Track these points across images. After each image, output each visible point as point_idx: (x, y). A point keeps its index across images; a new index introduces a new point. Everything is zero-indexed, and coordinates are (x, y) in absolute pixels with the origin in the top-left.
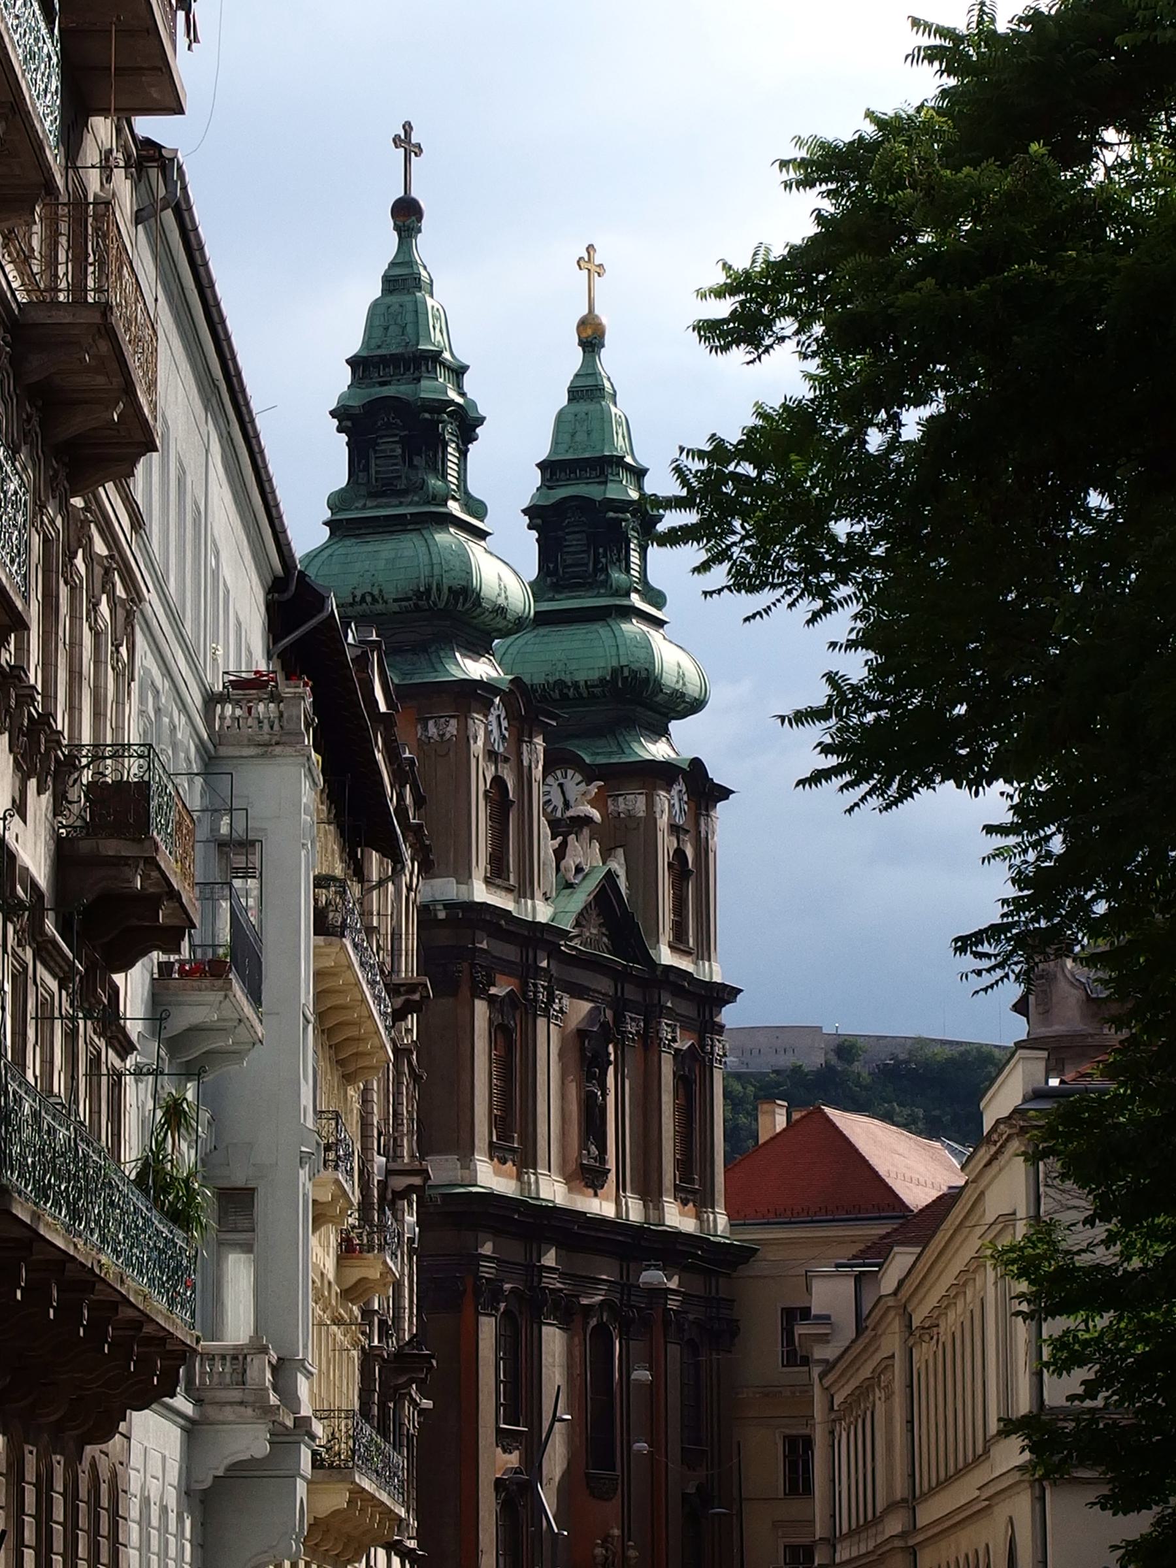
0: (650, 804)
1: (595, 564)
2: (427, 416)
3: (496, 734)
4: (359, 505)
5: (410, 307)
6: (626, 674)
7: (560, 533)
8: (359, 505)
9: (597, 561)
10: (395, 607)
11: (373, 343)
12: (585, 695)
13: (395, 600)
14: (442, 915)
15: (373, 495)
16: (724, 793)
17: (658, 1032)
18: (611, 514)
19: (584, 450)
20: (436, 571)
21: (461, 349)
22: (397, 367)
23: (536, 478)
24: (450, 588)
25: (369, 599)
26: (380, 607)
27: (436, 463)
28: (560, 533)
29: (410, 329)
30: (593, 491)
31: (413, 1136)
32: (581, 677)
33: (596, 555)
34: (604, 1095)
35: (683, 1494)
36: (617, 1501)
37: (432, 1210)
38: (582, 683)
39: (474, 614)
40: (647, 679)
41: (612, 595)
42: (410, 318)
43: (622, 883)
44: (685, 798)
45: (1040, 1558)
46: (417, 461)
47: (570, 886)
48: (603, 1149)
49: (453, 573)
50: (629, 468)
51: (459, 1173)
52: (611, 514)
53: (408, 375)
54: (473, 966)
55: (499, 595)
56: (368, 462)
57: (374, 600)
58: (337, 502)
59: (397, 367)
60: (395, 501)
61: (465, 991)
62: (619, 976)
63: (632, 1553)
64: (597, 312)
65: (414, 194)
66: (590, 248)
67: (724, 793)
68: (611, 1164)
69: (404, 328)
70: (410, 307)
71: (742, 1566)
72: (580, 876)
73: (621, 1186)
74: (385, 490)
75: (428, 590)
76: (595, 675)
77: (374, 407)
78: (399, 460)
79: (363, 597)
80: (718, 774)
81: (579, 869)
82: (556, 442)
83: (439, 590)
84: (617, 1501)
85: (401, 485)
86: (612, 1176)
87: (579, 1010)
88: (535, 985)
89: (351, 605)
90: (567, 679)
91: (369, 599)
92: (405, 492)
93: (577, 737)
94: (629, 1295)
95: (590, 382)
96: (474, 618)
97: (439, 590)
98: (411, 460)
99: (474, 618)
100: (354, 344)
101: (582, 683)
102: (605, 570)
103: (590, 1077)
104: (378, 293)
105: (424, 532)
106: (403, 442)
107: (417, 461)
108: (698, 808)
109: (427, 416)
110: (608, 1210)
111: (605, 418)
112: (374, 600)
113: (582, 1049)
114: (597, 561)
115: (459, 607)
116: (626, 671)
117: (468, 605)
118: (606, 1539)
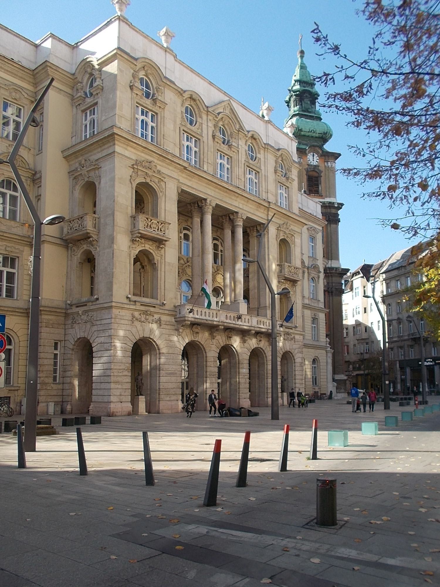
13: (319, 133)
25: (313, 131)
57: (314, 132)
89: (308, 132)
91: (313, 131)
112: (314, 132)
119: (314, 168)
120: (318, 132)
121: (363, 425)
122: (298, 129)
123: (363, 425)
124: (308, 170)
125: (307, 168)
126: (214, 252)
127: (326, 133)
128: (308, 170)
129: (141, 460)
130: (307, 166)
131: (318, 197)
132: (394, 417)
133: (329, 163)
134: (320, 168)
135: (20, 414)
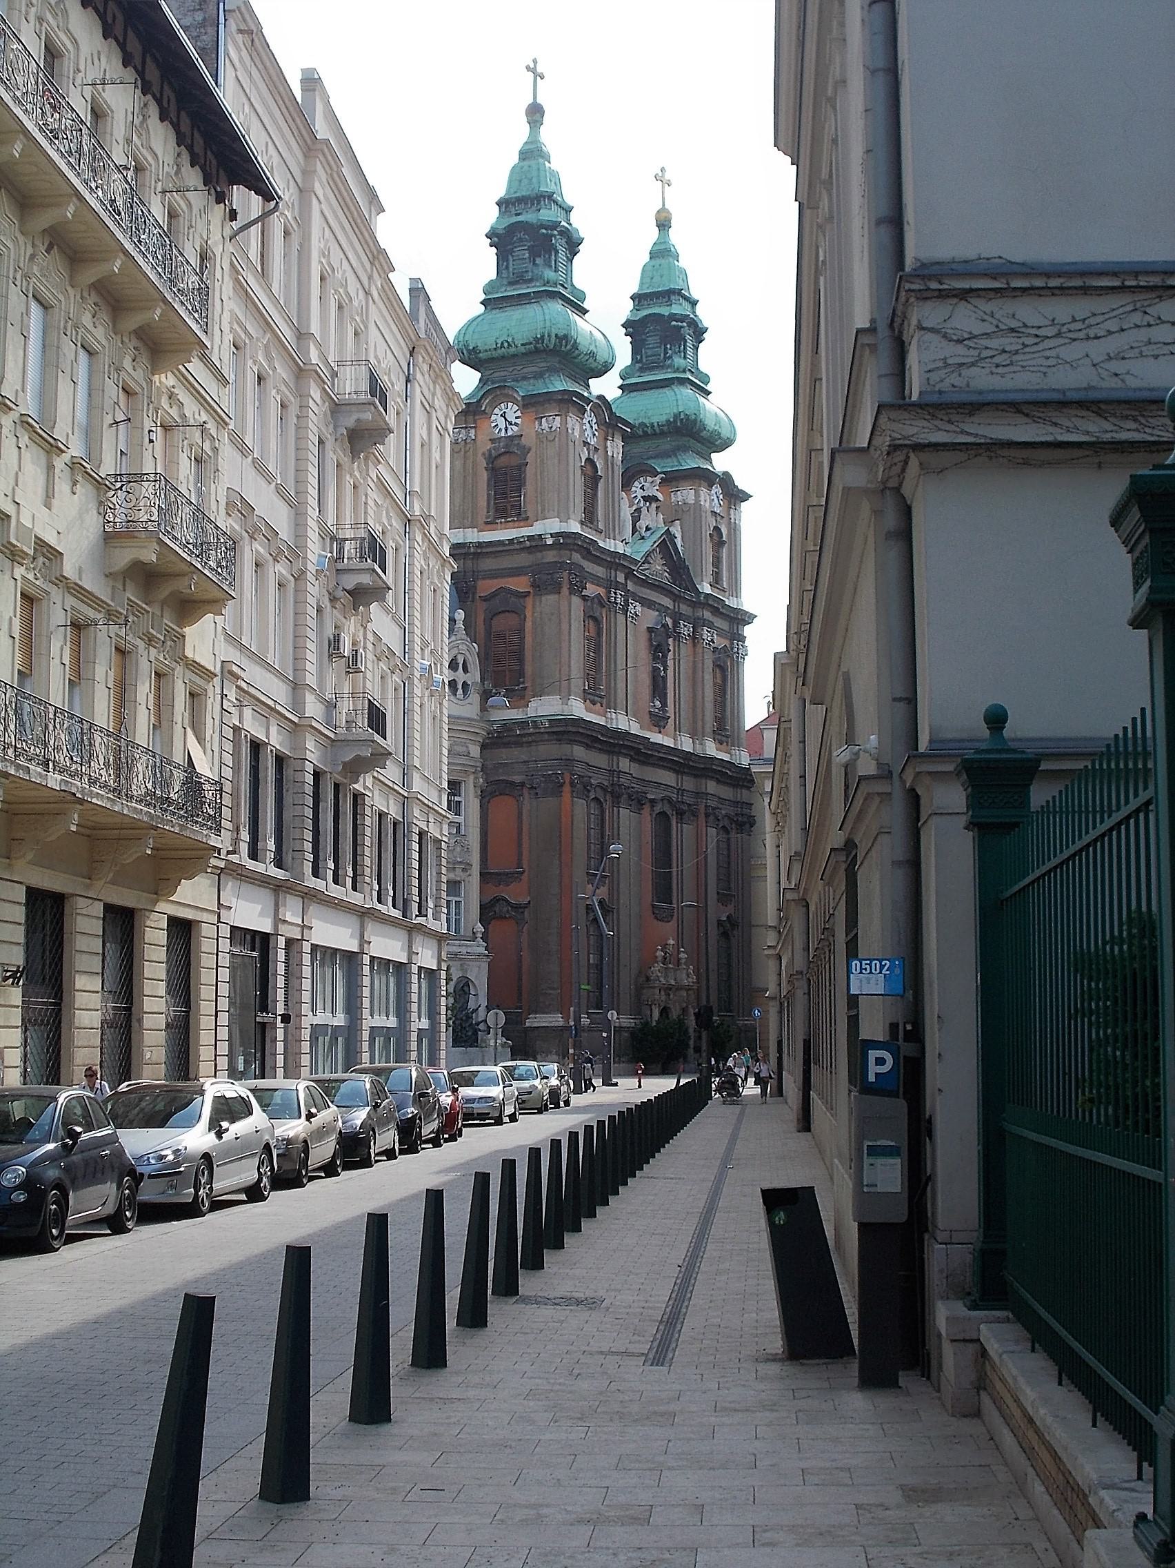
0: (697, 495)
1: (665, 354)
2: (544, 231)
3: (588, 432)
4: (503, 289)
5: (534, 167)
6: (682, 417)
7: (644, 337)
8: (503, 289)
9: (666, 353)
10: (522, 349)
11: (512, 191)
12: (658, 431)
13: (522, 345)
14: (549, 542)
15: (511, 284)
16: (745, 497)
17: (702, 635)
18: (674, 323)
19: (659, 287)
20: (548, 324)
21: (569, 197)
22: (526, 204)
23: (630, 305)
24: (556, 335)
25: (506, 345)
26: (513, 350)
27: (550, 261)
28: (644, 337)
29: (534, 180)
30: (665, 311)
31: (684, 759)
32: (655, 420)
33: (666, 348)
34: (665, 670)
35: (719, 921)
36: (673, 923)
37: (542, 730)
38: (656, 424)
39: (574, 355)
40: (696, 420)
41: (675, 372)
42: (534, 173)
43: (679, 542)
44: (721, 497)
45: (884, 209)
46: (538, 261)
47: (643, 538)
48: (664, 704)
49: (559, 326)
50: (687, 299)
51: (560, 707)
52: (674, 323)
53: (534, 208)
54: (570, 574)
55: (590, 344)
56: (508, 264)
57: (509, 345)
58: (489, 288)
59: (526, 204)
60: (525, 286)
61: (565, 591)
62: (676, 598)
63: (682, 955)
64: (666, 206)
65: (538, 101)
66: (663, 170)
67: (745, 497)
68: (671, 713)
69: (531, 179)
70: (534, 167)
71: (1, 879)
72: (649, 532)
73: (678, 728)
74: (519, 279)
75: (543, 336)
76: (663, 419)
77: (512, 229)
78: (527, 261)
79: (502, 343)
80: (741, 483)
81: (648, 529)
82: (642, 284)
83: (549, 336)
84: (673, 923)
85: (529, 276)
86: (671, 721)
87: (649, 618)
88: (615, 593)
89: (495, 349)
90: (646, 421)
91: (506, 345)
92: (531, 280)
93: (654, 458)
94: (682, 795)
95: (663, 247)
96: (575, 358)
97: (549, 336)
98: (534, 260)
99: (575, 358)
100: (501, 191)
101: (656, 424)
102: (670, 357)
103: (655, 658)
104: (517, 160)
105: (542, 303)
106: (530, 249)
107: (538, 261)
108: (730, 503)
109: (544, 231)
110: (669, 742)
111: (671, 267)
112: (509, 345)
113: (650, 640)
114: (666, 353)
115: (563, 348)
116: (682, 417)
117: (568, 347)
118: (665, 946)
119: (506, 446)
120: (519, 343)
121: (1136, 1453)
122: (468, 351)
123: (1136, 1453)
124: (490, 455)
125: (490, 451)
126: (1156, 1162)
127: (543, 336)
128: (490, 455)
129: (98, 918)
130: (489, 446)
131: (516, 524)
132: (856, 336)
133: (544, 420)
134: (523, 441)
135: (890, 793)
